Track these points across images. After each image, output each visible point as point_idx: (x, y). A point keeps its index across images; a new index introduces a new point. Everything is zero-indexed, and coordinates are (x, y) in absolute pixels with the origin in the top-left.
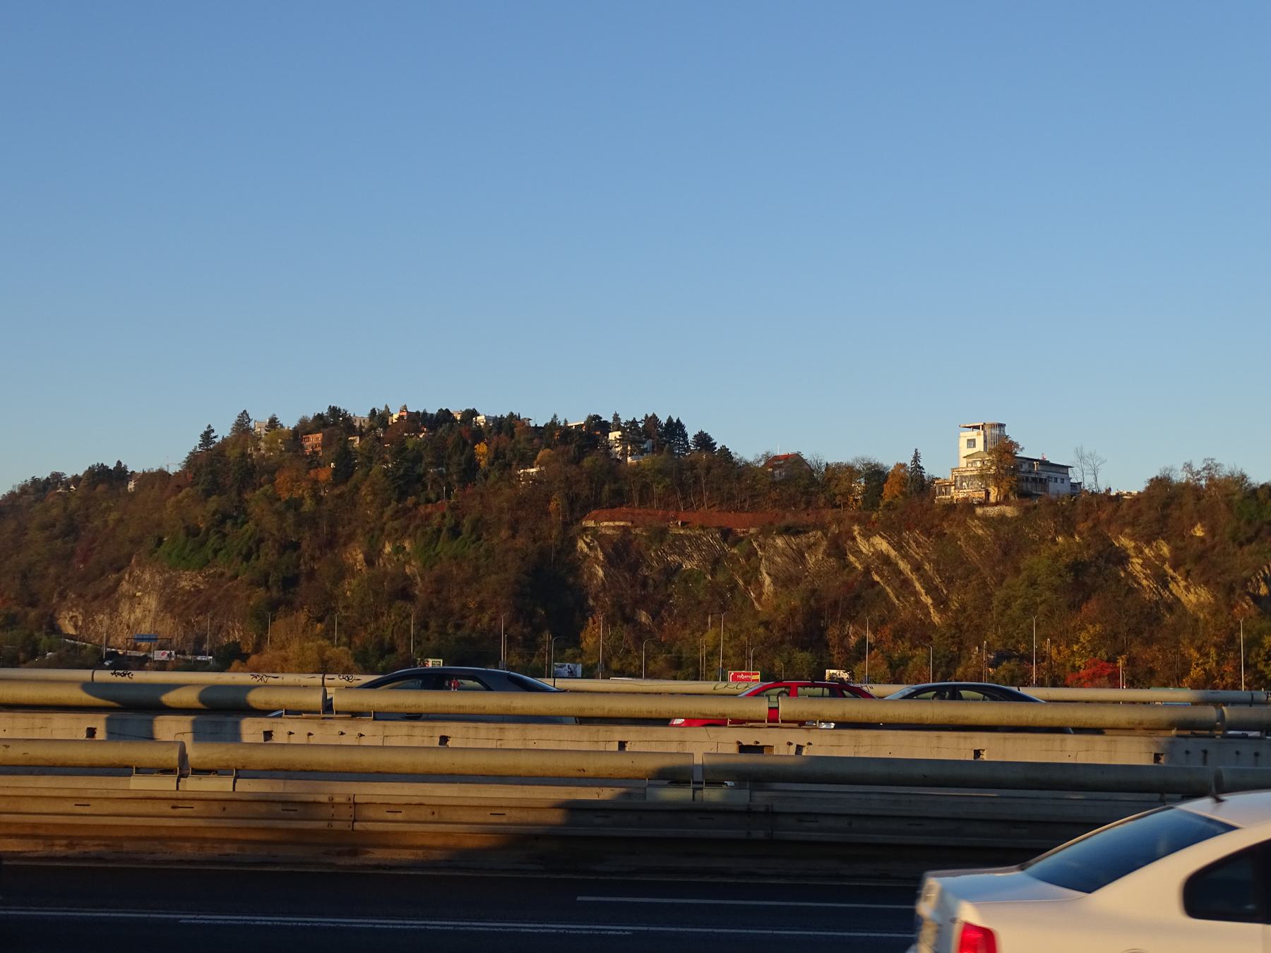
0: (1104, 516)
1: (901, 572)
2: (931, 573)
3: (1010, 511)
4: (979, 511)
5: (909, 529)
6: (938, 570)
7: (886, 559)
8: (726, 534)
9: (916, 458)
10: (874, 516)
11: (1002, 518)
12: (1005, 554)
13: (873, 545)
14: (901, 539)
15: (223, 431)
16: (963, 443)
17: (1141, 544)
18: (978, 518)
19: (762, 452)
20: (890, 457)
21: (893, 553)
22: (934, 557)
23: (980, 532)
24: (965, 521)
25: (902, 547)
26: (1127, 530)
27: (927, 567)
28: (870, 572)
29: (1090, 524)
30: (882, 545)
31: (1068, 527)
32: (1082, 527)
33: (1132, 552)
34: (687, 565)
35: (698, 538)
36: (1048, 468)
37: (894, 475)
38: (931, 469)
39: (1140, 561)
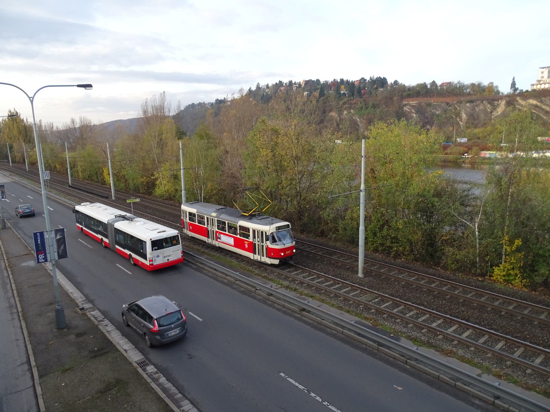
7: (536, 106)
8: (447, 104)
9: (513, 84)
15: (254, 88)
21: (539, 104)
34: (437, 113)
35: (440, 105)
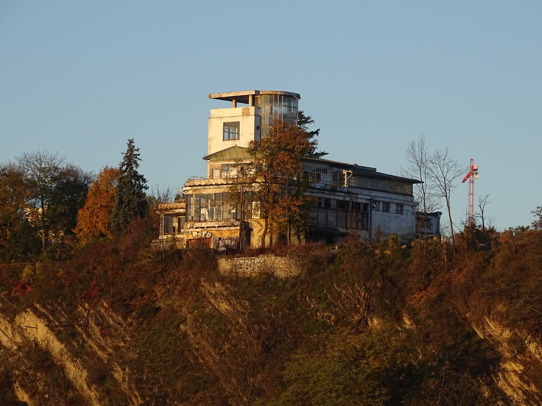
0: (459, 279)
1: (69, 385)
2: (125, 386)
3: (282, 266)
4: (225, 265)
5: (88, 298)
6: (139, 381)
7: (40, 357)
9: (131, 157)
10: (27, 271)
11: (268, 277)
12: (267, 350)
13: (21, 331)
14: (75, 318)
16: (216, 130)
17: (523, 334)
18: (222, 280)
19: (20, 155)
20: (93, 159)
21: (57, 346)
22: (132, 355)
23: (224, 306)
24: (197, 285)
25: (74, 335)
26: (500, 308)
27: (118, 375)
28: (10, 385)
29: (432, 293)
30: (37, 329)
31: (390, 298)
32: (418, 299)
33: (505, 350)
36: (369, 183)
37: (97, 191)
38: (161, 180)
39: (519, 368)
